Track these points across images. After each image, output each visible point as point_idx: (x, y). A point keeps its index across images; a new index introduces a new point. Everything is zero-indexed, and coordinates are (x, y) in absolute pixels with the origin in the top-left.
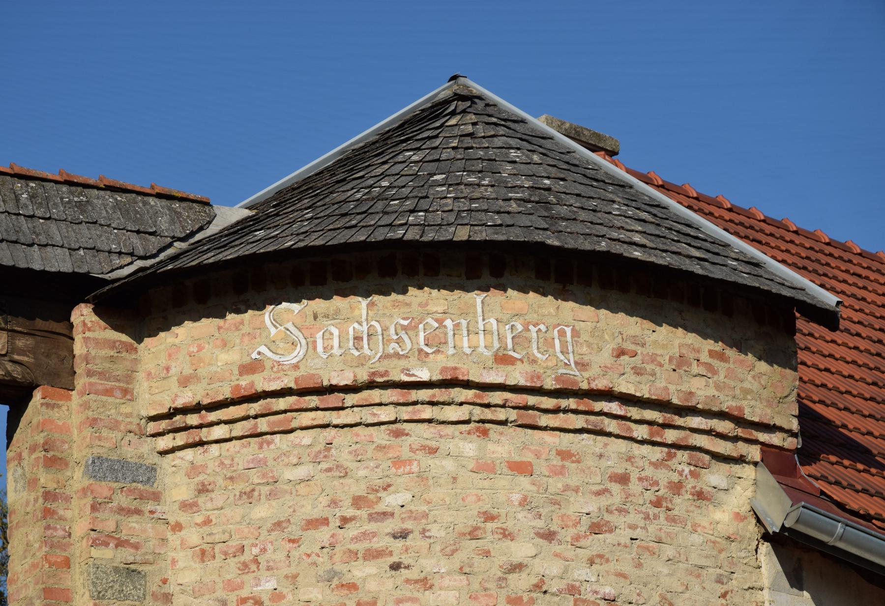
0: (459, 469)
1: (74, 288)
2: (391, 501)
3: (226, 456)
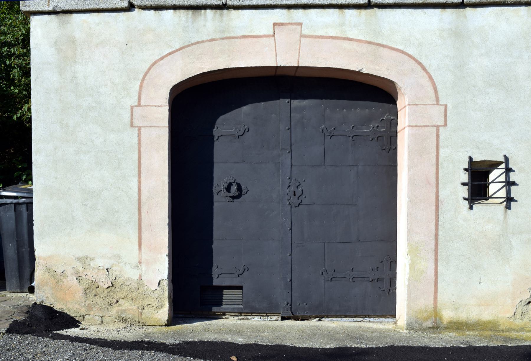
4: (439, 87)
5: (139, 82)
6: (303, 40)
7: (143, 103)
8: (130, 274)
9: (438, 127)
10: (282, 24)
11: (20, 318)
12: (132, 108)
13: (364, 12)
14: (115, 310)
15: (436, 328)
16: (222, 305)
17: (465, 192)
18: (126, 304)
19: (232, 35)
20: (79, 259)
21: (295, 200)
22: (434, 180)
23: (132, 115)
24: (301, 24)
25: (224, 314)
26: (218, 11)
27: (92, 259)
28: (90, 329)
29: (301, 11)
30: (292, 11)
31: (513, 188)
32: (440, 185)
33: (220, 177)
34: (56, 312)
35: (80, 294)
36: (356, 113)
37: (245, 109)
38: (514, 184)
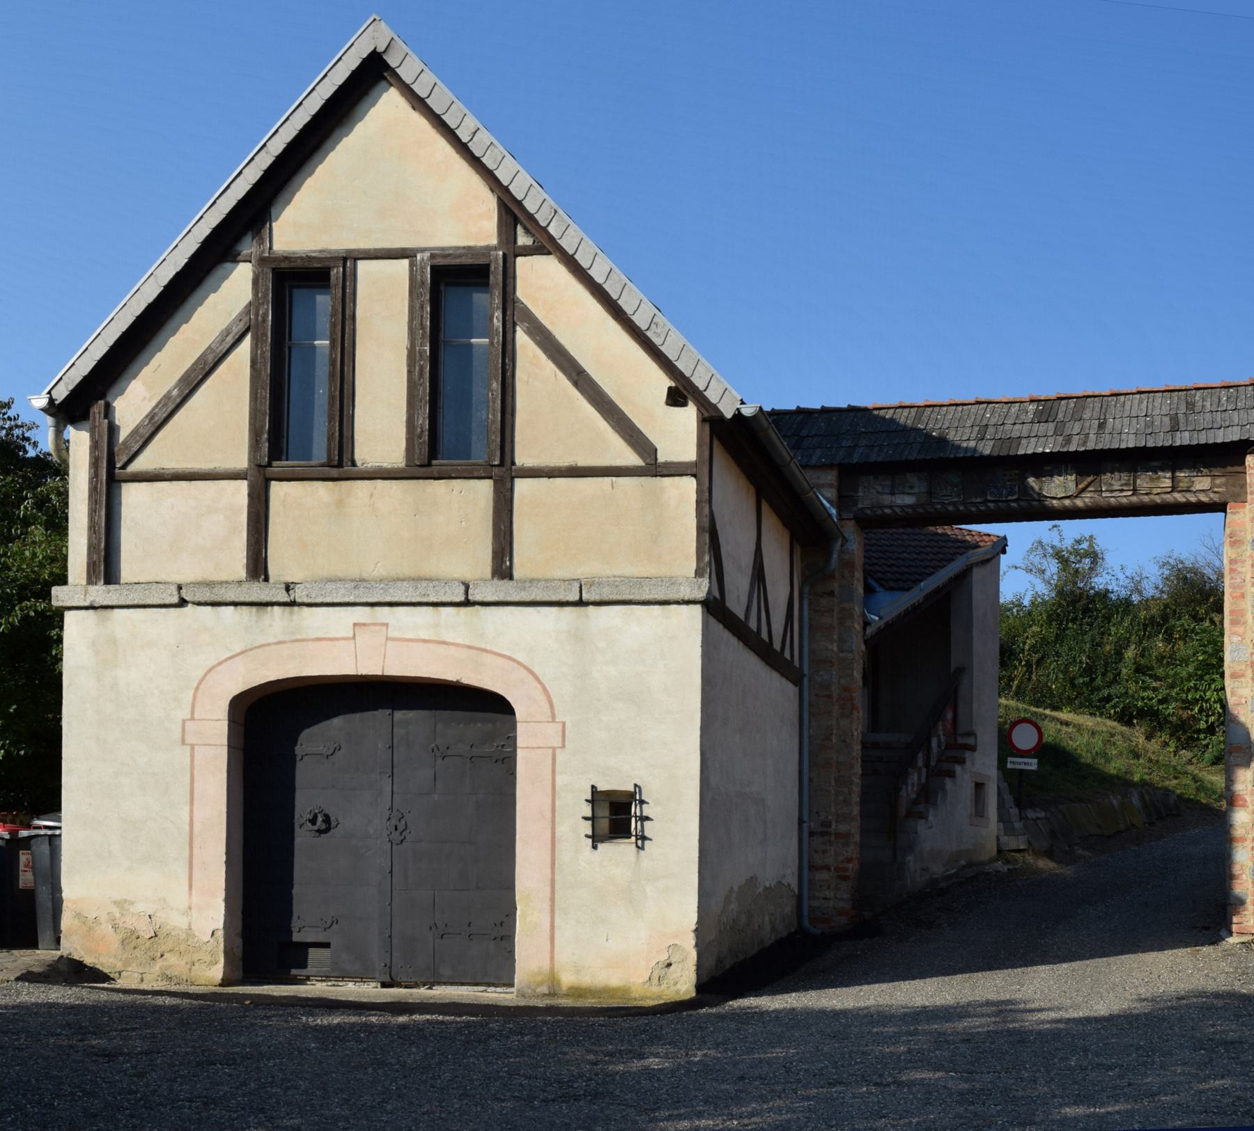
4: (555, 701)
5: (192, 692)
6: (389, 643)
7: (196, 716)
8: (177, 922)
9: (554, 749)
10: (364, 625)
11: (35, 969)
12: (184, 721)
13: (463, 610)
14: (159, 964)
15: (552, 994)
16: (305, 967)
17: (587, 828)
18: (171, 959)
19: (304, 636)
20: (116, 903)
21: (396, 836)
22: (549, 815)
23: (183, 730)
24: (387, 625)
25: (308, 978)
26: (288, 609)
27: (132, 903)
28: (121, 983)
29: (387, 609)
30: (377, 608)
31: (646, 824)
32: (557, 820)
33: (304, 804)
34: (86, 966)
35: (116, 944)
36: (472, 727)
37: (337, 721)
38: (647, 818)
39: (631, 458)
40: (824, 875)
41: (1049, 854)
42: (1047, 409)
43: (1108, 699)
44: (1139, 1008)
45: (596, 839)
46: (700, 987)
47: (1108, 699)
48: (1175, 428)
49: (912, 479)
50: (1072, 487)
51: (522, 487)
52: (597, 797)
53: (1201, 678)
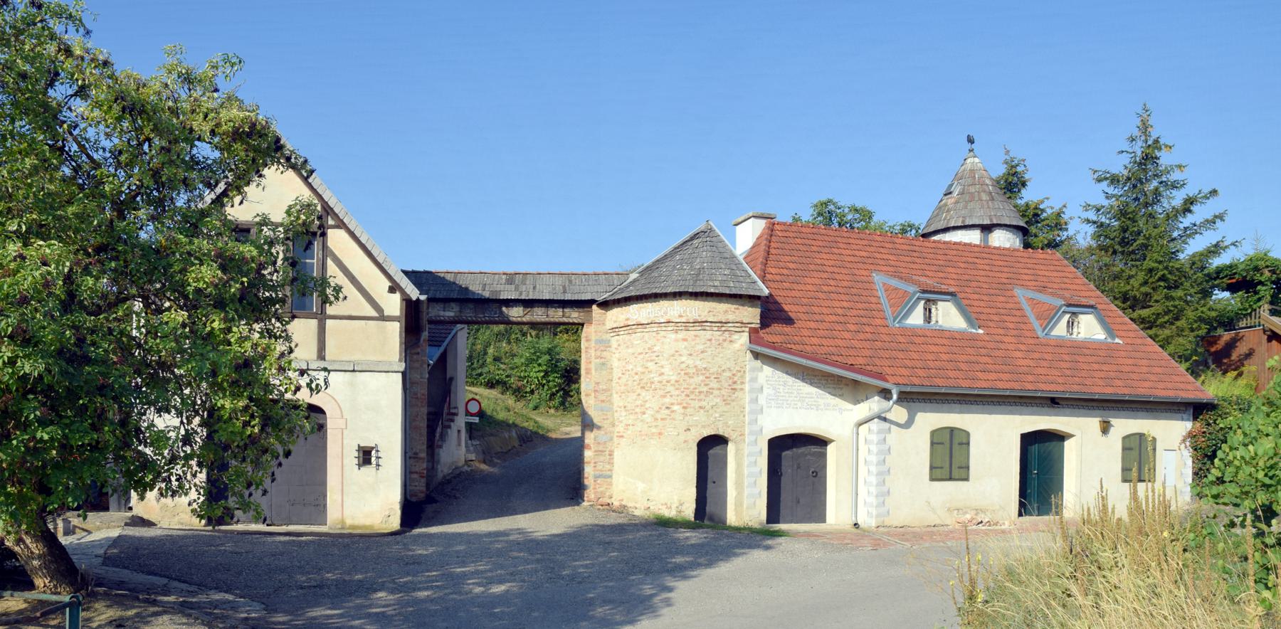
0: (671, 341)
1: (590, 302)
2: (656, 349)
3: (623, 337)
17: (356, 461)
39: (374, 313)
40: (415, 476)
41: (484, 462)
42: (511, 278)
43: (480, 375)
44: (570, 530)
45: (360, 466)
46: (402, 525)
47: (480, 375)
48: (565, 292)
49: (453, 305)
50: (521, 313)
51: (329, 322)
52: (360, 449)
53: (527, 365)
